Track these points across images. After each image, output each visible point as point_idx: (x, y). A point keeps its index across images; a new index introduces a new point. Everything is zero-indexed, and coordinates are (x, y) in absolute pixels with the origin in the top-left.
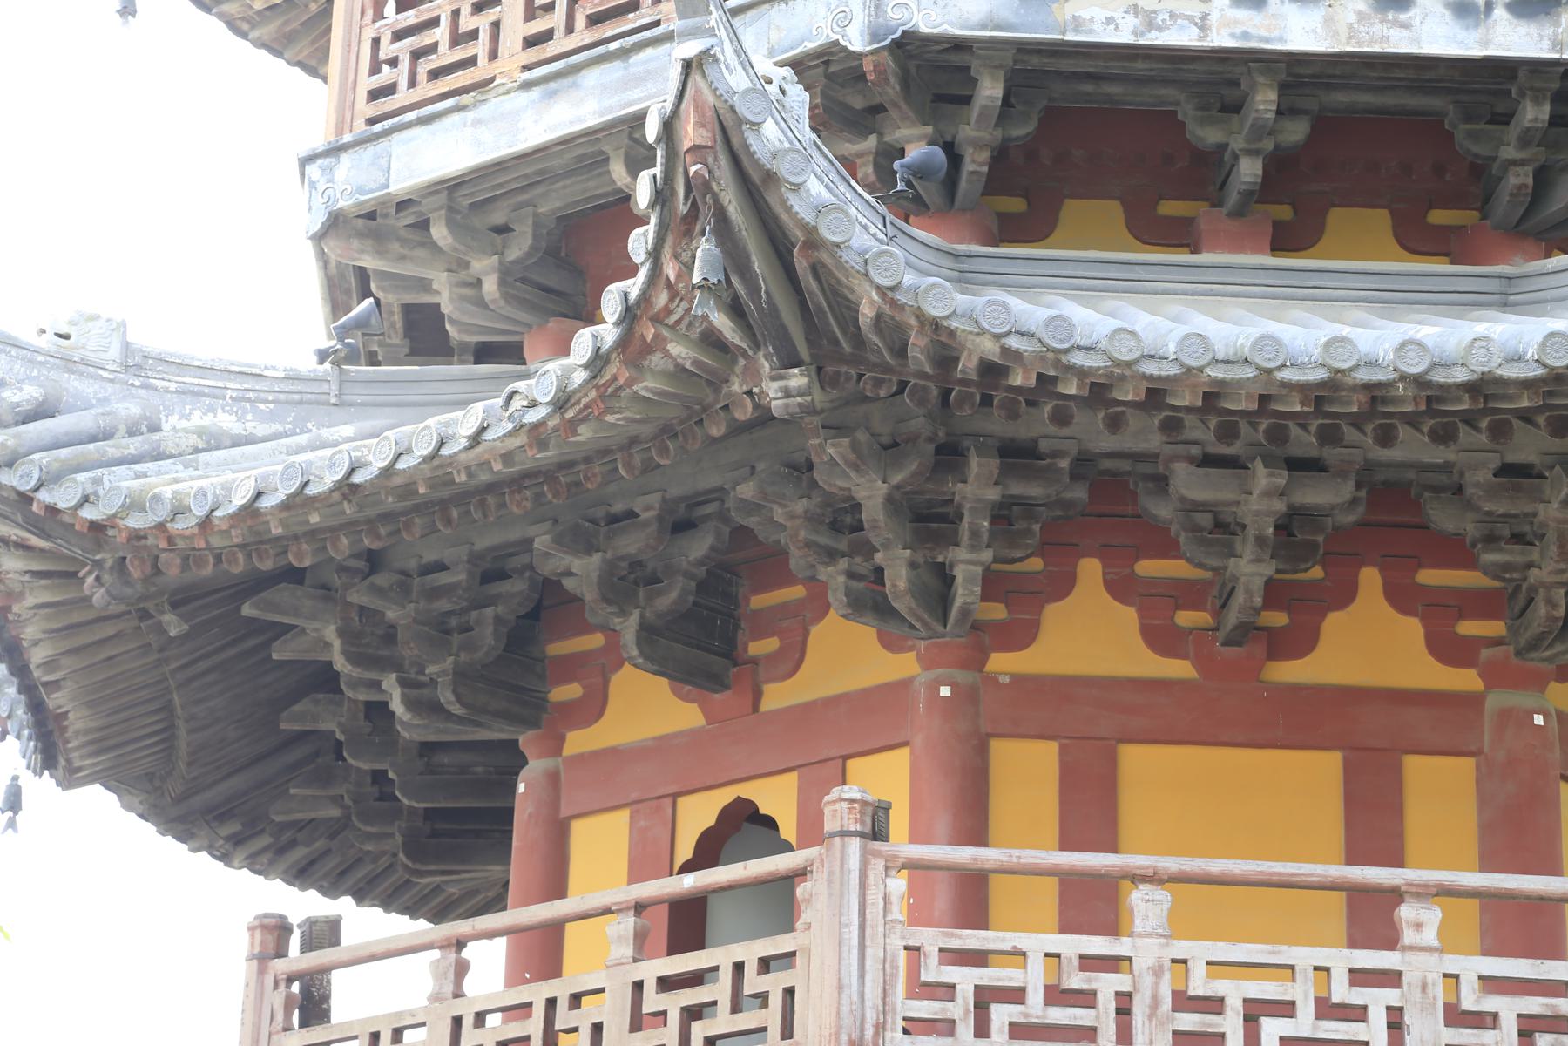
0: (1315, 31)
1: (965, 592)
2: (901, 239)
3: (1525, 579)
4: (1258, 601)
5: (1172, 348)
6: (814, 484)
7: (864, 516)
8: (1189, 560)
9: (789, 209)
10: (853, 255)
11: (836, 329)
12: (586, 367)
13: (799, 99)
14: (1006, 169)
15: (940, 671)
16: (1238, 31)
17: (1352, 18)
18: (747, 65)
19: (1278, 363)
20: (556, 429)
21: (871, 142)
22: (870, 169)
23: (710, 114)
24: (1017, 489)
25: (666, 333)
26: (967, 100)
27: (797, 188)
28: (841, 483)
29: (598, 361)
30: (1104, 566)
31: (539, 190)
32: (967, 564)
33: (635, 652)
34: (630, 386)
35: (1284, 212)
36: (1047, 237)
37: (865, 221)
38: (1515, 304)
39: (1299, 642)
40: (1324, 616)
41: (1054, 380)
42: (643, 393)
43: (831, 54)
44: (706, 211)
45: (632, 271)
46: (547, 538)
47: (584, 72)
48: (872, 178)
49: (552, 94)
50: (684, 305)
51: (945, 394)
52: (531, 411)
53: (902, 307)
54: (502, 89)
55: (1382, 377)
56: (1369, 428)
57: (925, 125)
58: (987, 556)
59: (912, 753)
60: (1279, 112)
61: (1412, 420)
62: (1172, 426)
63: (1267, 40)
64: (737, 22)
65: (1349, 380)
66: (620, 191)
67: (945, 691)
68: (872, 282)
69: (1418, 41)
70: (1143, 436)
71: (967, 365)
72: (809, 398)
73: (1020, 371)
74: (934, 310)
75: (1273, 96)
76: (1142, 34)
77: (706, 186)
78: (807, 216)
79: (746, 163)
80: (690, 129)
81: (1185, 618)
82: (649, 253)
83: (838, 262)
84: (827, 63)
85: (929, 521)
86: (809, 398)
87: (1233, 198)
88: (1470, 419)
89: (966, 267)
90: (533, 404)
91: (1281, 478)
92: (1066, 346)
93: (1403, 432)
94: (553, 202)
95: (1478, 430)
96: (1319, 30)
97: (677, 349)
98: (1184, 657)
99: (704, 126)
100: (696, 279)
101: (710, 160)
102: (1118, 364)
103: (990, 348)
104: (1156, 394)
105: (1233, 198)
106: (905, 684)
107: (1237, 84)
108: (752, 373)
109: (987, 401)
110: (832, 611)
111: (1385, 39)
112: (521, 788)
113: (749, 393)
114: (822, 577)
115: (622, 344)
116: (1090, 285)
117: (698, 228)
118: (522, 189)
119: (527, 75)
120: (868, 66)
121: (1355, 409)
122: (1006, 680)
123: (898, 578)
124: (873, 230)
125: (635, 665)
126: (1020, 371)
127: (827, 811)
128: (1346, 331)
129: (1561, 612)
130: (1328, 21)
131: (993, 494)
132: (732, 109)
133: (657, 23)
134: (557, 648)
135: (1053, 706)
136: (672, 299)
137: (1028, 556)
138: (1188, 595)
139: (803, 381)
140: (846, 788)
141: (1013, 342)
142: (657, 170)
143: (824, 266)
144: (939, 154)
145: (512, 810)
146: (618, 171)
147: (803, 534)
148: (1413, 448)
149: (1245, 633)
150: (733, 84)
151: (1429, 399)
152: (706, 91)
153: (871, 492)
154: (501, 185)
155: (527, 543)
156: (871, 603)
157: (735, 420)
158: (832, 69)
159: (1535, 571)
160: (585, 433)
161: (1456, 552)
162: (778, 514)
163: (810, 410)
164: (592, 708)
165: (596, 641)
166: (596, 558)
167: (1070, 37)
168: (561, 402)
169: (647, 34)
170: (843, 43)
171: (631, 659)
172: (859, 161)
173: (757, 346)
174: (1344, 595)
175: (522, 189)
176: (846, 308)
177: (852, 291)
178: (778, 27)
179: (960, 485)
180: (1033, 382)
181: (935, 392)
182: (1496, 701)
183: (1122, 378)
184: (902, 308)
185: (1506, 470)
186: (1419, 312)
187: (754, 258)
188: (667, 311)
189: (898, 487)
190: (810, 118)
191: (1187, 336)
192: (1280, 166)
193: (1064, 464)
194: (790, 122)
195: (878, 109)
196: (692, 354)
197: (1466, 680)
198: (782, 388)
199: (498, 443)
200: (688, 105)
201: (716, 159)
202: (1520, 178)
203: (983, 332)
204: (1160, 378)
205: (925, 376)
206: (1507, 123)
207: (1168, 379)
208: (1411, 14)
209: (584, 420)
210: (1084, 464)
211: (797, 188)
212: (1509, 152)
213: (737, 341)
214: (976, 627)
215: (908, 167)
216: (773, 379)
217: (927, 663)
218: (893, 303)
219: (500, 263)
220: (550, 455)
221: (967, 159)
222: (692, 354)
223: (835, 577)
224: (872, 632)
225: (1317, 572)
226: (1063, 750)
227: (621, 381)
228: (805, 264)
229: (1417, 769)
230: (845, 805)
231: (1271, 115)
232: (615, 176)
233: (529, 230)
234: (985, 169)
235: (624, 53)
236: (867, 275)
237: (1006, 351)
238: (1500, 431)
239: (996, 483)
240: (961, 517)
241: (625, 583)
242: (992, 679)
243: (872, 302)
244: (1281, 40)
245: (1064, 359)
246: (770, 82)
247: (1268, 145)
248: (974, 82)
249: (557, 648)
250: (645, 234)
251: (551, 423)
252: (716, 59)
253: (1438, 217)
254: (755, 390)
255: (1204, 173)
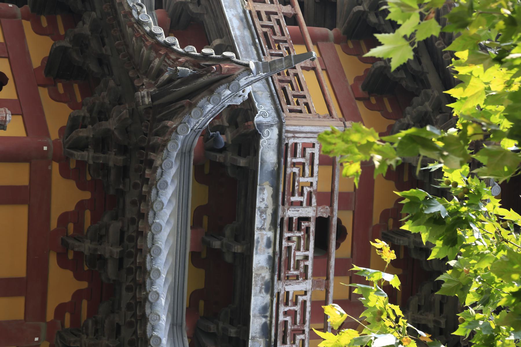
0: (259, 263)
1: (78, 155)
2: (194, 134)
3: (83, 333)
4: (76, 249)
5: (157, 221)
6: (114, 105)
7: (103, 122)
8: (90, 227)
9: (202, 98)
10: (187, 119)
11: (163, 113)
12: (151, 31)
13: (238, 101)
14: (218, 167)
15: (52, 147)
16: (260, 240)
17: (263, 275)
18: (248, 85)
19: (152, 254)
20: (130, 21)
21: (227, 124)
22: (218, 124)
23: (232, 73)
24: (113, 172)
25: (162, 58)
26: (239, 155)
27: (209, 101)
28: (114, 114)
29: (153, 35)
30: (88, 200)
31: (212, 16)
32: (88, 155)
33: (57, 45)
34: (145, 46)
35: (204, 255)
36: (197, 180)
37: (200, 122)
38: (173, 328)
39: (63, 263)
40: (71, 270)
41: (147, 184)
42: (142, 50)
43: (254, 111)
44: (201, 71)
45: (182, 47)
46: (95, 16)
47: (249, 31)
48: (215, 124)
49: (241, 20)
50: (171, 64)
51: (143, 148)
52: (136, 13)
53: (170, 135)
54: (243, 3)
55: (148, 287)
56: (132, 284)
57: (232, 141)
58: (91, 162)
59: (24, 137)
60: (234, 253)
61: (134, 297)
62: (133, 221)
63: (256, 249)
64: (264, 81)
65: (147, 276)
66: (211, 42)
67: (45, 148)
68: (179, 125)
69: (255, 295)
70: (130, 213)
71: (152, 155)
72: (141, 104)
73: (150, 172)
74: (170, 145)
75: (239, 251)
76: (259, 210)
77: (209, 71)
78: (200, 104)
79: (217, 84)
80: (227, 66)
81: (71, 226)
82: (188, 52)
83: (184, 114)
84: (251, 110)
85: (102, 143)
86: (141, 104)
87: (208, 239)
88: (134, 315)
89: (187, 154)
90: (138, 13)
91: (116, 256)
92: (158, 187)
93: (131, 294)
94: (208, 20)
95: (131, 317)
96: (259, 265)
97: (157, 61)
98: (58, 226)
99: (228, 71)
100: (178, 68)
101: (217, 73)
102: (152, 204)
103: (158, 162)
104: (143, 216)
105: (208, 239)
106: (48, 135)
107: (244, 239)
108: (149, 86)
109: (141, 162)
110: (72, 111)
111: (256, 285)
112: (10, 5)
113: (143, 85)
114: (83, 108)
115: (158, 43)
116: (181, 194)
117: (196, 68)
118: (212, 10)
119: (248, 12)
120: (250, 123)
121: (137, 279)
122: (49, 168)
123: (83, 133)
124: (197, 125)
125: (53, 46)
126: (150, 172)
127: (2, 109)
128: (164, 276)
129: (72, 345)
130: (262, 268)
131: (111, 164)
132: (234, 80)
133: (264, 55)
134: (59, 19)
135: (41, 184)
136: (173, 60)
137: (91, 176)
138: (79, 226)
139: (147, 102)
140: (10, 116)
141: (159, 171)
142: (214, 55)
143: (184, 109)
144: (221, 146)
145: (4, 2)
146: (217, 42)
147: (97, 102)
148: (126, 297)
149: (66, 246)
150: (242, 80)
151: (140, 302)
152: (239, 71)
153: (111, 124)
154: (213, 3)
155: (94, 9)
156: (74, 124)
157: (134, 80)
158: (249, 111)
159: (85, 337)
160: (129, 30)
161: (92, 312)
162: (104, 94)
163: (137, 104)
164: (39, 30)
165: (62, 32)
166: (89, 33)
167: (258, 187)
168: (139, 23)
169: (261, 52)
170: (257, 115)
171: (55, 44)
172: (220, 120)
173: (158, 87)
174: (78, 277)
175: (212, 10)
176: (170, 117)
177: (176, 119)
178: (262, 94)
179: (114, 153)
180: (147, 177)
181: (143, 145)
182: (43, 325)
183: (148, 205)
184: (170, 134)
185: (119, 327)
186: (171, 299)
187: (186, 87)
188: (169, 58)
189: (113, 133)
190: (234, 105)
191: (161, 226)
192: (217, 254)
193: (121, 187)
194: (230, 99)
195: (237, 126)
196: (155, 66)
197: (50, 316)
198: (144, 95)
199: (125, 1)
200: (234, 66)
201: (217, 75)
202: (213, 328)
203: (163, 161)
204: (148, 217)
205: (149, 142)
206: (230, 324)
207: (147, 220)
208: (264, 293)
209: (133, 30)
210: (121, 193)
211: (209, 101)
212: (221, 325)
213: (160, 81)
214: (67, 159)
215: (217, 136)
216: (147, 93)
217: (55, 142)
218: (172, 132)
219: (188, 2)
220: (122, 19)
221: (221, 155)
222: (155, 66)
223: (83, 112)
224: (65, 125)
225: (86, 268)
226: (25, 187)
227: (146, 43)
228: (185, 103)
229: (20, 301)
230: (4, 115)
231: (233, 250)
232: (216, 41)
233: (198, 12)
234: (217, 161)
235: (254, 44)
236: (181, 123)
237: (156, 168)
238: (131, 324)
239: (115, 165)
240: (104, 153)
241: (80, 42)
242: (50, 163)
243: (172, 125)
244: (257, 253)
245: (154, 187)
246: (243, 92)
247: (224, 250)
248: (245, 157)
249: (59, 19)
250: (194, 51)
251: (132, 19)
252: (249, 75)
253: (202, 303)
254: (144, 87)
255: (216, 231)
